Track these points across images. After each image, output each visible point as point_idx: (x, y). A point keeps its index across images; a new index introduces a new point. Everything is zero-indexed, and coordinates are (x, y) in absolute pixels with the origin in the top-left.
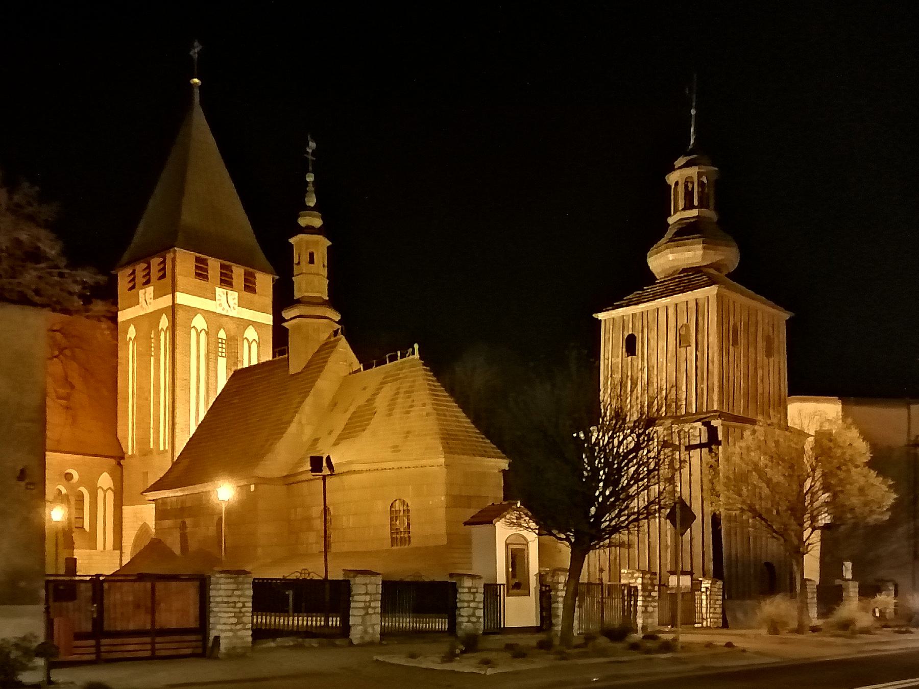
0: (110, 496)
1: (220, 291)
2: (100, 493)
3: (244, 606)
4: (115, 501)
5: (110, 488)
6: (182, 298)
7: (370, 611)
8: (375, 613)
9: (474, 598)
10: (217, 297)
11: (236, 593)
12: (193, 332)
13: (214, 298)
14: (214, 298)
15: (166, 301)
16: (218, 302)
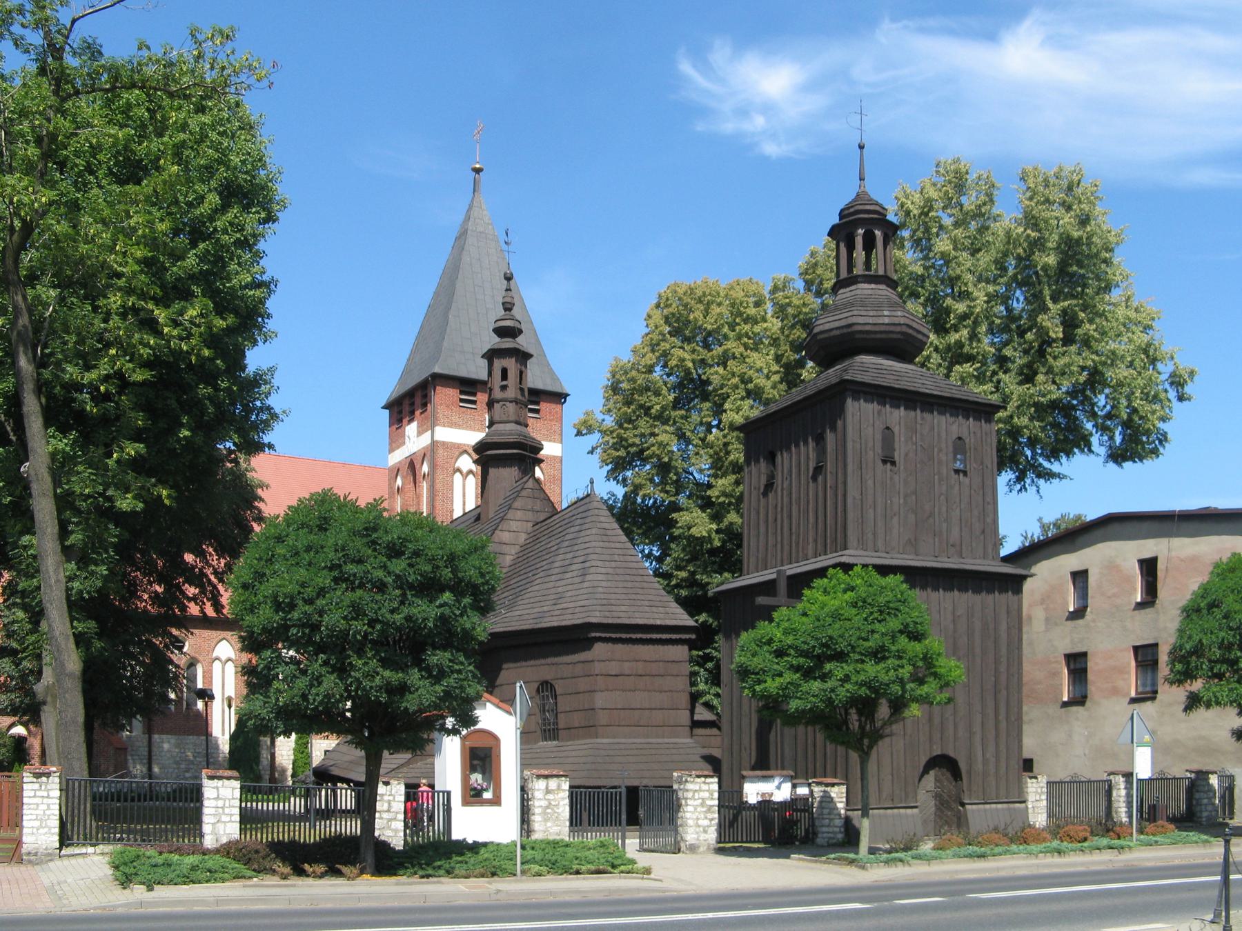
3: (49, 808)
7: (224, 818)
8: (231, 821)
9: (390, 806)
11: (38, 793)
15: (425, 440)
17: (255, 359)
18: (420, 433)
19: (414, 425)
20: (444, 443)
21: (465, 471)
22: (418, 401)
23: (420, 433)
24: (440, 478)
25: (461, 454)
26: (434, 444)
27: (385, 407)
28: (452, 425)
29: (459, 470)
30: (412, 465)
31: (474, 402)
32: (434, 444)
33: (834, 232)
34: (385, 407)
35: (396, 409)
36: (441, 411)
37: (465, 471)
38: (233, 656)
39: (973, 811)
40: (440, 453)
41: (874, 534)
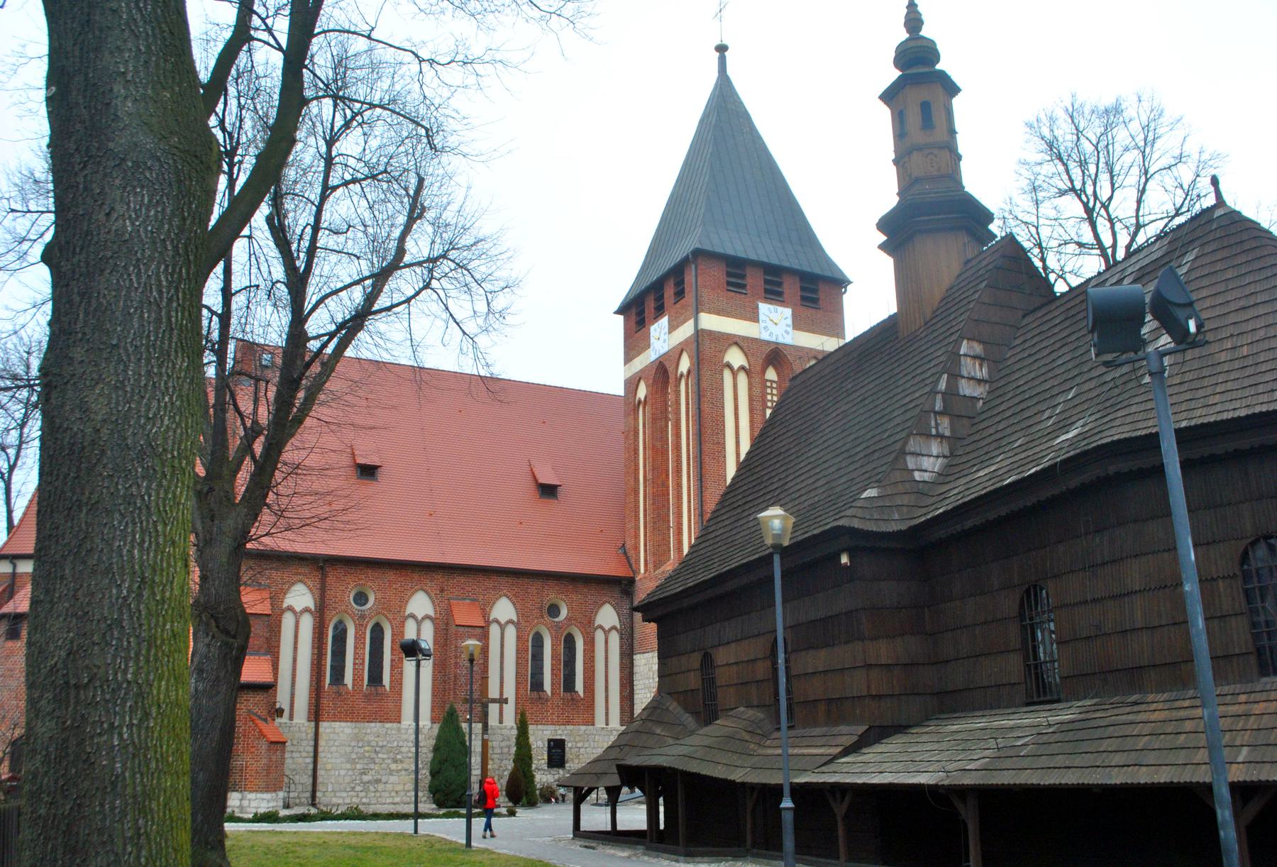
0: (615, 639)
1: (764, 308)
2: (599, 636)
4: (621, 647)
5: (614, 628)
6: (710, 322)
10: (762, 317)
12: (727, 375)
13: (755, 318)
14: (755, 318)
15: (686, 330)
16: (762, 325)
17: (896, 74)
18: (672, 328)
19: (664, 321)
20: (710, 333)
21: (736, 367)
22: (669, 292)
23: (672, 328)
24: (706, 373)
25: (730, 345)
26: (699, 334)
27: (618, 312)
28: (719, 312)
29: (729, 366)
30: (662, 373)
31: (743, 286)
32: (699, 334)
33: (623, 310)
34: (618, 312)
35: (634, 311)
36: (705, 294)
37: (736, 367)
38: (431, 613)
39: (238, 835)
40: (707, 345)
41: (1136, 703)
